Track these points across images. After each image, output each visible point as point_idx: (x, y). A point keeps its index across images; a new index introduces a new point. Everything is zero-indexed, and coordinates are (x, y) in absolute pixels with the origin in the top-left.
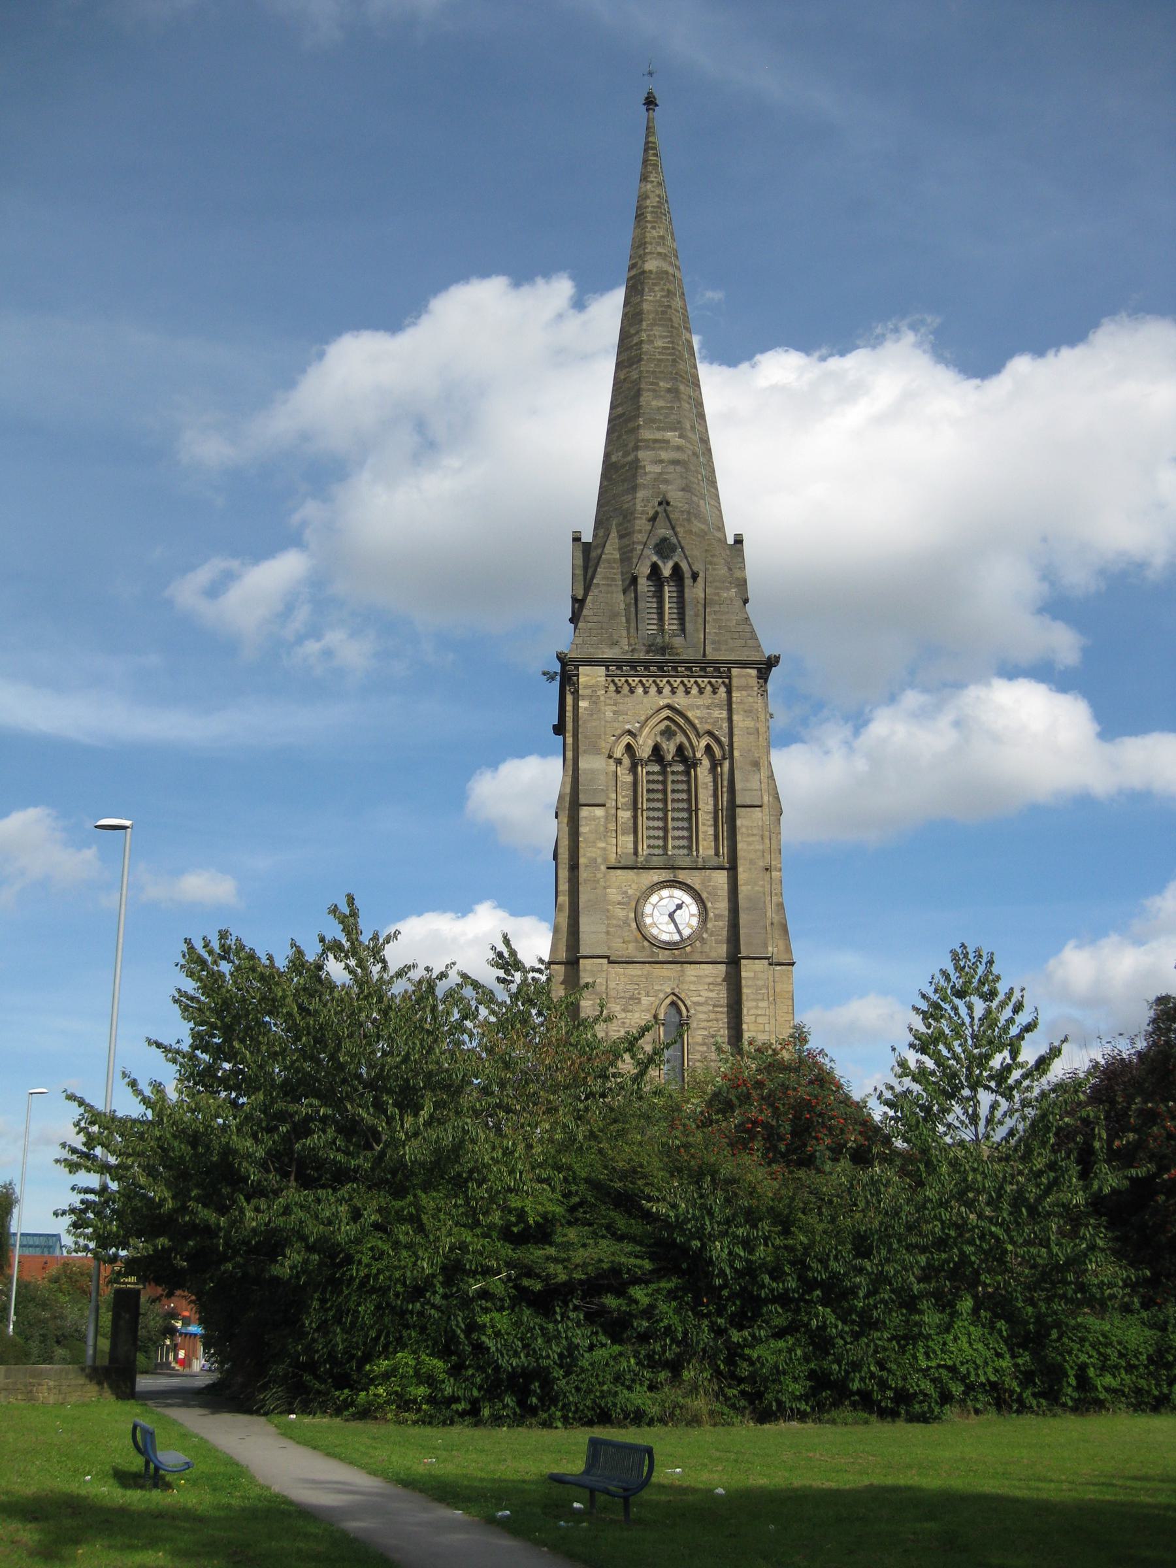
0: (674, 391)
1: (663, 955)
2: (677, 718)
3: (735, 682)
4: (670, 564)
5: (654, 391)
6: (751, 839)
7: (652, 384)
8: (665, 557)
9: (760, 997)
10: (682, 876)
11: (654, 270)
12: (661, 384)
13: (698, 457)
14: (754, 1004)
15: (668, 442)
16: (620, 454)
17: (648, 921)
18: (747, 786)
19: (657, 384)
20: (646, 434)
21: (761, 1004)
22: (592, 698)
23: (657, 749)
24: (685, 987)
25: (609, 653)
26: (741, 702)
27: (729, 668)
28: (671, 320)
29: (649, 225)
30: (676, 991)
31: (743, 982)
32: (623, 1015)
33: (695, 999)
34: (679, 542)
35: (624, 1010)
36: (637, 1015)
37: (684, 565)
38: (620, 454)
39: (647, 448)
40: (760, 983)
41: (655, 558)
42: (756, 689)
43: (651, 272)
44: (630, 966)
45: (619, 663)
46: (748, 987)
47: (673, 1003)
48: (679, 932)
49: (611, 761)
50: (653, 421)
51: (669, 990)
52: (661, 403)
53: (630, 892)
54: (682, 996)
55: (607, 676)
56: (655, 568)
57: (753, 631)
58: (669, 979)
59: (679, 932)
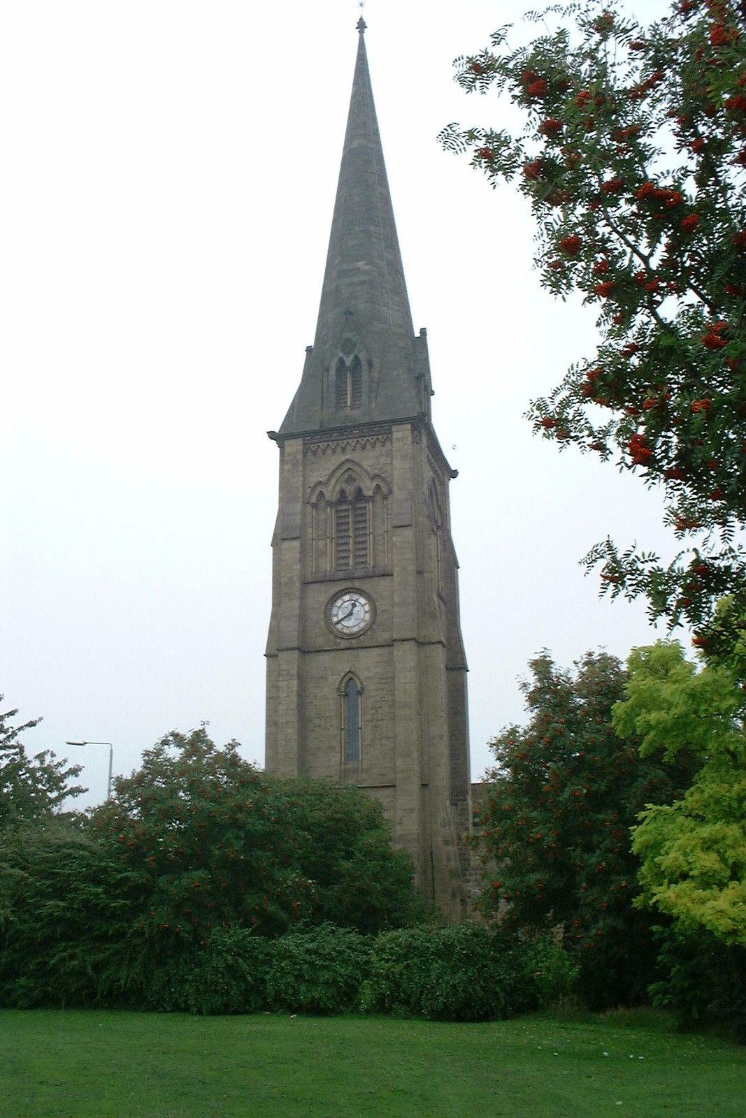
1: (344, 644)
4: (352, 357)
8: (347, 353)
10: (357, 584)
13: (384, 276)
15: (358, 269)
33: (366, 674)
37: (362, 356)
41: (341, 354)
42: (410, 438)
49: (309, 506)
55: (304, 444)
56: (341, 361)
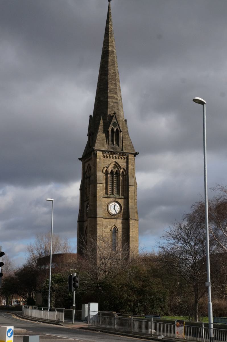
0: (115, 84)
1: (113, 217)
2: (117, 165)
3: (129, 157)
4: (116, 128)
5: (111, 83)
6: (132, 193)
7: (111, 82)
8: (115, 127)
9: (133, 227)
10: (117, 200)
11: (111, 50)
12: (113, 82)
14: (132, 229)
15: (114, 97)
16: (103, 98)
17: (110, 209)
18: (131, 181)
19: (112, 82)
20: (109, 95)
21: (133, 229)
22: (100, 159)
23: (112, 171)
24: (117, 224)
25: (103, 149)
26: (130, 162)
27: (128, 154)
28: (115, 65)
29: (110, 37)
30: (115, 225)
31: (130, 224)
32: (104, 230)
34: (118, 123)
35: (105, 229)
36: (107, 230)
38: (103, 98)
39: (110, 98)
40: (133, 224)
41: (113, 127)
43: (110, 51)
44: (106, 219)
45: (105, 151)
46: (131, 225)
47: (115, 228)
48: (116, 212)
50: (111, 91)
51: (114, 225)
52: (113, 87)
53: (106, 203)
54: (116, 226)
57: (133, 146)
58: (114, 222)
59: (116, 212)
